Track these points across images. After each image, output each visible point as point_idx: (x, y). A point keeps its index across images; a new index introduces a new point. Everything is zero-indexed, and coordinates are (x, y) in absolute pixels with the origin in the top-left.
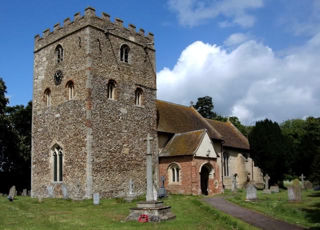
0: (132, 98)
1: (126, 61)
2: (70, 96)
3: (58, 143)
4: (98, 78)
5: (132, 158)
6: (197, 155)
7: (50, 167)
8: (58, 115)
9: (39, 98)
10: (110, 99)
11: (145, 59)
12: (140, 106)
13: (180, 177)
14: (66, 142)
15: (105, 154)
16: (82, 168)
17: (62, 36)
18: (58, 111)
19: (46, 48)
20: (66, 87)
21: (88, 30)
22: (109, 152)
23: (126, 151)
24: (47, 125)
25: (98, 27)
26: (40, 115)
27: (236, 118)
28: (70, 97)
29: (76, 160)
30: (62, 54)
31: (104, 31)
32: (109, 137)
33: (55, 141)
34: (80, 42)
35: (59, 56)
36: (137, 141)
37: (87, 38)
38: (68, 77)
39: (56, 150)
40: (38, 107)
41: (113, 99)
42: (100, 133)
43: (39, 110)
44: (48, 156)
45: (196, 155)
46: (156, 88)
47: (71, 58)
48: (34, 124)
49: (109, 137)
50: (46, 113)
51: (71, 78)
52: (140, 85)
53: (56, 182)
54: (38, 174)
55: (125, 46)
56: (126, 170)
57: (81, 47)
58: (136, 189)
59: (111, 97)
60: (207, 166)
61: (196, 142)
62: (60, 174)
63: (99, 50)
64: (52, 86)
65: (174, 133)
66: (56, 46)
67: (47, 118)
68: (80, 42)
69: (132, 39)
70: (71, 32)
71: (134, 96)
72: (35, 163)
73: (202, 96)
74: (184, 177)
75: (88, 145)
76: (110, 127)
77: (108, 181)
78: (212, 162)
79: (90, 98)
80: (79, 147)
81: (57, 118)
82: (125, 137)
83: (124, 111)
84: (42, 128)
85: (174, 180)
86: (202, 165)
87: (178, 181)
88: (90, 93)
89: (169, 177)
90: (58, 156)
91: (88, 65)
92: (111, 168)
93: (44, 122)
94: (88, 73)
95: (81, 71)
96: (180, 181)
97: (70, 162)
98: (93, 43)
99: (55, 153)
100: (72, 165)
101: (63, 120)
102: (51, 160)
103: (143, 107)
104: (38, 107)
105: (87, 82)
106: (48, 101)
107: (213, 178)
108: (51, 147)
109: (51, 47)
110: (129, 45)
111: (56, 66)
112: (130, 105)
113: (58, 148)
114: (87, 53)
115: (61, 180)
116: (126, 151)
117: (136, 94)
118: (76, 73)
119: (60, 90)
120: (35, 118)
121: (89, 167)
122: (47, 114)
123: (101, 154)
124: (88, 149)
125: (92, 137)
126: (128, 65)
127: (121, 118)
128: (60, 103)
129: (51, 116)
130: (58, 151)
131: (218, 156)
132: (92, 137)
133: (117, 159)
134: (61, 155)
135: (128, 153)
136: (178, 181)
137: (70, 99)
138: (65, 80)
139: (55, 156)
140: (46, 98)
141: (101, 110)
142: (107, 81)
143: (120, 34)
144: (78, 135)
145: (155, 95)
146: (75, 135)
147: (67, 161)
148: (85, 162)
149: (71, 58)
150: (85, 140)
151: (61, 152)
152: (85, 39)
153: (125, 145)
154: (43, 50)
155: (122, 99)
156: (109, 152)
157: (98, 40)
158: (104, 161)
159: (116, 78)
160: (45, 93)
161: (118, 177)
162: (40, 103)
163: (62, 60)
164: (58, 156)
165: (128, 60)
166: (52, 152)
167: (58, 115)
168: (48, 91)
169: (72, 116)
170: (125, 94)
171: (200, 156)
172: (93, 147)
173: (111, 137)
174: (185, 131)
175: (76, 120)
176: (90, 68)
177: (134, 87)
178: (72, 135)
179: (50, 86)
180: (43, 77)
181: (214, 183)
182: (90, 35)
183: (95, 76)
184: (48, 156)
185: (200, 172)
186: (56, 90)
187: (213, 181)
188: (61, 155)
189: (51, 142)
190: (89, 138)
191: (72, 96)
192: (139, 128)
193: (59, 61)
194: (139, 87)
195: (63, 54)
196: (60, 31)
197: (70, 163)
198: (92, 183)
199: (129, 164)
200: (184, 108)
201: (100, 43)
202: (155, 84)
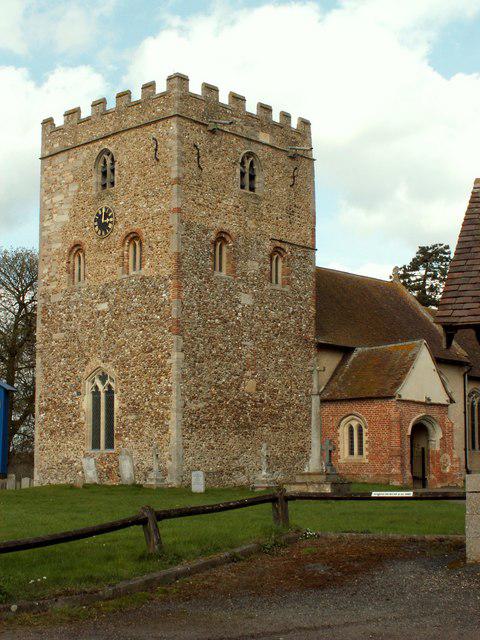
0: (262, 271)
1: (252, 189)
2: (131, 265)
3: (102, 365)
4: (195, 229)
5: (262, 401)
6: (403, 398)
7: (83, 419)
8: (104, 306)
9: (55, 264)
10: (217, 274)
11: (291, 181)
12: (278, 287)
13: (365, 446)
14: (122, 364)
15: (206, 391)
16: (160, 421)
17: (111, 130)
18: (104, 296)
19: (71, 152)
20: (123, 244)
21: (173, 127)
22: (217, 386)
23: (250, 385)
24: (76, 325)
25: (194, 118)
26: (59, 303)
27: (244, 100)
28: (131, 270)
29: (147, 403)
30: (113, 171)
31: (207, 125)
32: (215, 357)
33: (96, 362)
34: (156, 150)
35: (104, 174)
36: (271, 366)
37: (173, 143)
38: (127, 224)
39: (98, 382)
40: (53, 286)
41: (224, 274)
42: (198, 346)
43: (55, 292)
44: (79, 394)
45: (400, 396)
46: (314, 245)
47: (134, 182)
48: (43, 322)
49: (215, 357)
50: (73, 299)
51: (136, 227)
52: (281, 241)
53: (96, 451)
54: (52, 432)
55: (250, 154)
56: (249, 427)
57: (158, 160)
58: (273, 462)
59: (220, 270)
60: (425, 422)
61: (404, 368)
62: (106, 433)
63: (196, 168)
64: (90, 237)
65: (350, 345)
66: (97, 151)
67: (76, 311)
68: (156, 150)
69: (264, 138)
70: (135, 125)
71: (268, 266)
72: (42, 410)
73: (437, 76)
74: (372, 445)
75: (174, 372)
76: (218, 334)
77: (213, 448)
78: (435, 413)
79: (179, 274)
80: (154, 375)
81: (103, 313)
82: (249, 355)
83: (246, 300)
84: (62, 331)
85: (351, 452)
86: (414, 420)
87: (361, 452)
88: (179, 263)
89: (340, 446)
90: (103, 395)
91: (175, 203)
92: (219, 421)
93: (69, 318)
94: (174, 219)
95: (158, 214)
96: (365, 453)
97: (134, 407)
98: (184, 154)
99: (96, 387)
100: (136, 414)
101: (116, 316)
102: (86, 402)
103: (285, 289)
104: (53, 286)
105: (174, 240)
106: (76, 272)
107: (438, 448)
108: (85, 374)
109: (84, 153)
110: (258, 150)
111: (100, 198)
112: (260, 286)
113: (103, 378)
114: (174, 175)
115: (110, 444)
116: (250, 385)
117: (271, 260)
118: (147, 216)
119: (108, 250)
120: (45, 309)
121: (174, 421)
122: (76, 303)
123: (201, 391)
124: (173, 380)
125: (182, 355)
126: (256, 197)
127: (240, 314)
128: (108, 279)
129: (88, 308)
130: (103, 383)
131: (452, 401)
132: (182, 355)
133: (232, 402)
134: (110, 393)
135: (254, 390)
136: (361, 452)
137: (132, 273)
138: (120, 230)
139: (96, 394)
140: (74, 266)
141: (200, 297)
142: (213, 235)
143: (239, 130)
144: (151, 350)
145: (244, 106)
146: (144, 350)
147: (124, 405)
148: (167, 408)
149: (134, 182)
150: (169, 361)
151: (109, 386)
152: (169, 145)
153: (248, 373)
154: (65, 155)
155: (244, 274)
156: (217, 386)
157: (195, 146)
158: (206, 407)
159: (232, 227)
160: (71, 251)
161: (233, 442)
162: (58, 276)
163: (113, 184)
164: (103, 395)
165: (257, 186)
166: (88, 387)
167: (104, 306)
168: (77, 249)
169: (136, 309)
170: (249, 263)
171: (408, 398)
172: (184, 376)
173: (220, 355)
174: (378, 342)
175: (146, 318)
176: (179, 210)
177: (268, 246)
178: (137, 350)
179: (83, 240)
180: (65, 218)
181: (441, 460)
182: (179, 137)
183: (189, 226)
184: (79, 394)
185: (409, 433)
186: (99, 249)
187: (439, 456)
188: (110, 393)
189: (86, 363)
190: (176, 357)
191: (138, 268)
192: (276, 335)
193: (104, 186)
194: (278, 244)
195: (116, 172)
196: (106, 118)
197: (134, 411)
198: (181, 451)
199: (256, 415)
200: (376, 284)
201: (198, 153)
202: (314, 236)
